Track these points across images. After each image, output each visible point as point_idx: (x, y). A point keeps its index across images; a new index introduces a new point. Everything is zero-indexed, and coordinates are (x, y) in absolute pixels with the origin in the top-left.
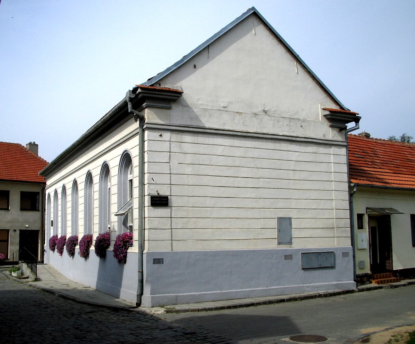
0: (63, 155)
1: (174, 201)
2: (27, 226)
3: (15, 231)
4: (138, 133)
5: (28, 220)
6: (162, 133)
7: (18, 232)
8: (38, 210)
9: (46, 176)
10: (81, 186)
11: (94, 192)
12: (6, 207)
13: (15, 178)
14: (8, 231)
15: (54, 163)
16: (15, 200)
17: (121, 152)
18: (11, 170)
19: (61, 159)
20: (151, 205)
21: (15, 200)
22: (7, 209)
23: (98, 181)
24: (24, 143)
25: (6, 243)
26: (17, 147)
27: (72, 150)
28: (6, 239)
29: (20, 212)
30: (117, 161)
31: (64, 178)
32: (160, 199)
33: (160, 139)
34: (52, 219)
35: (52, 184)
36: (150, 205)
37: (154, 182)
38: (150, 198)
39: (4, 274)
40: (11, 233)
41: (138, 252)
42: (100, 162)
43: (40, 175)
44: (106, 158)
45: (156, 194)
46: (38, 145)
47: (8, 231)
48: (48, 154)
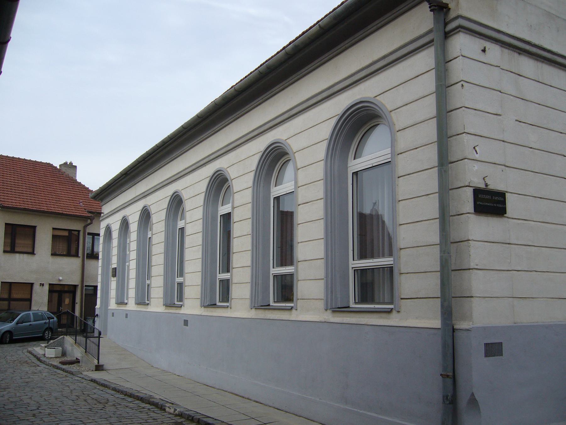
0: (150, 155)
1: (511, 202)
2: (61, 278)
3: (42, 285)
4: (432, 41)
5: (67, 270)
6: (489, 45)
7: (47, 288)
8: (77, 255)
9: (102, 200)
10: (134, 227)
11: (130, 242)
12: (30, 250)
13: (45, 208)
14: (32, 284)
15: (125, 174)
16: (44, 239)
17: (171, 193)
18: (40, 197)
19: (144, 163)
20: (475, 211)
21: (44, 239)
22: (33, 253)
23: (136, 229)
24: (57, 164)
25: (28, 303)
26: (45, 169)
27: (175, 141)
28: (29, 297)
29: (51, 258)
30: (165, 204)
31: (145, 195)
32: (492, 197)
33: (482, 57)
34: (114, 266)
35: (179, 175)
36: (473, 211)
37: (477, 157)
38: (473, 193)
39: (30, 352)
40: (36, 288)
41: (439, 326)
42: (139, 206)
43: (92, 198)
44: (126, 212)
45: (482, 186)
46: (76, 167)
47: (32, 284)
48: (93, 177)
